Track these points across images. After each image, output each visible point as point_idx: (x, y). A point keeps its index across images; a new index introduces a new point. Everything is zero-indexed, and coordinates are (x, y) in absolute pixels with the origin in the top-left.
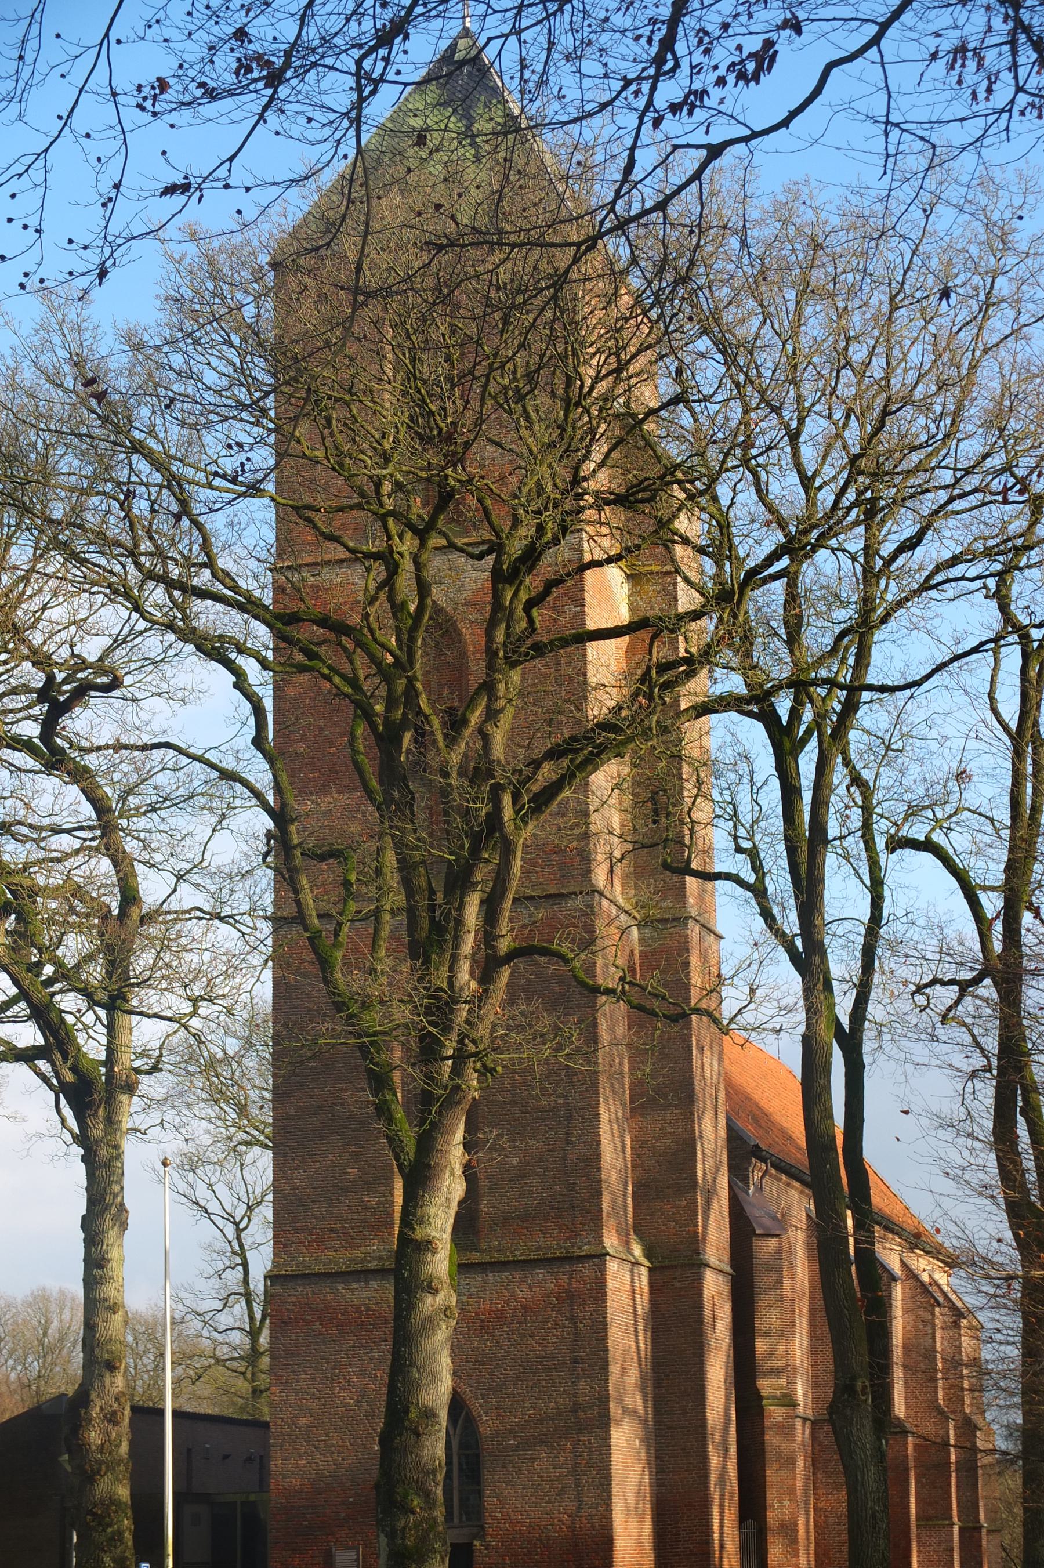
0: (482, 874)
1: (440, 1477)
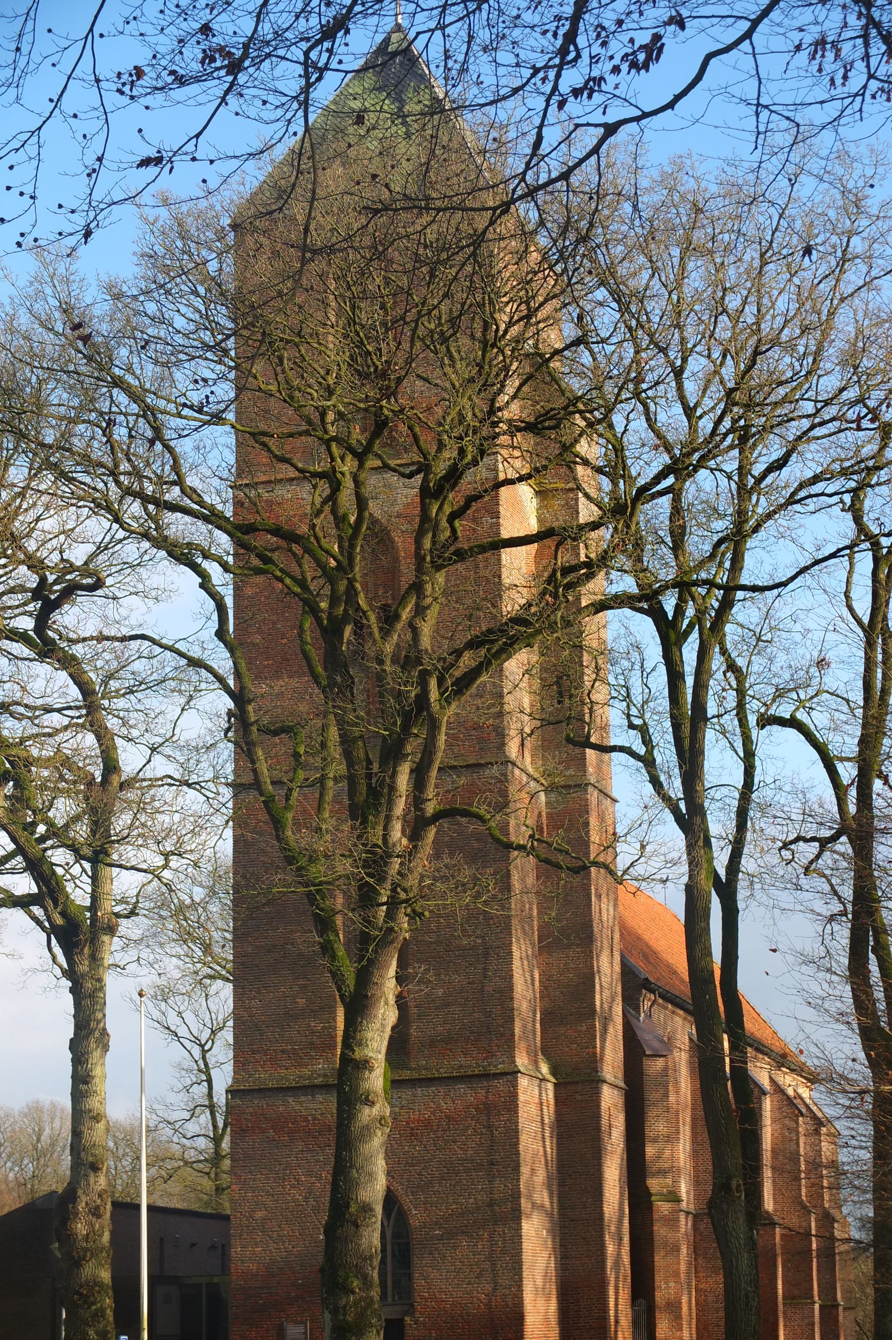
0: (412, 747)
1: (376, 1262)
